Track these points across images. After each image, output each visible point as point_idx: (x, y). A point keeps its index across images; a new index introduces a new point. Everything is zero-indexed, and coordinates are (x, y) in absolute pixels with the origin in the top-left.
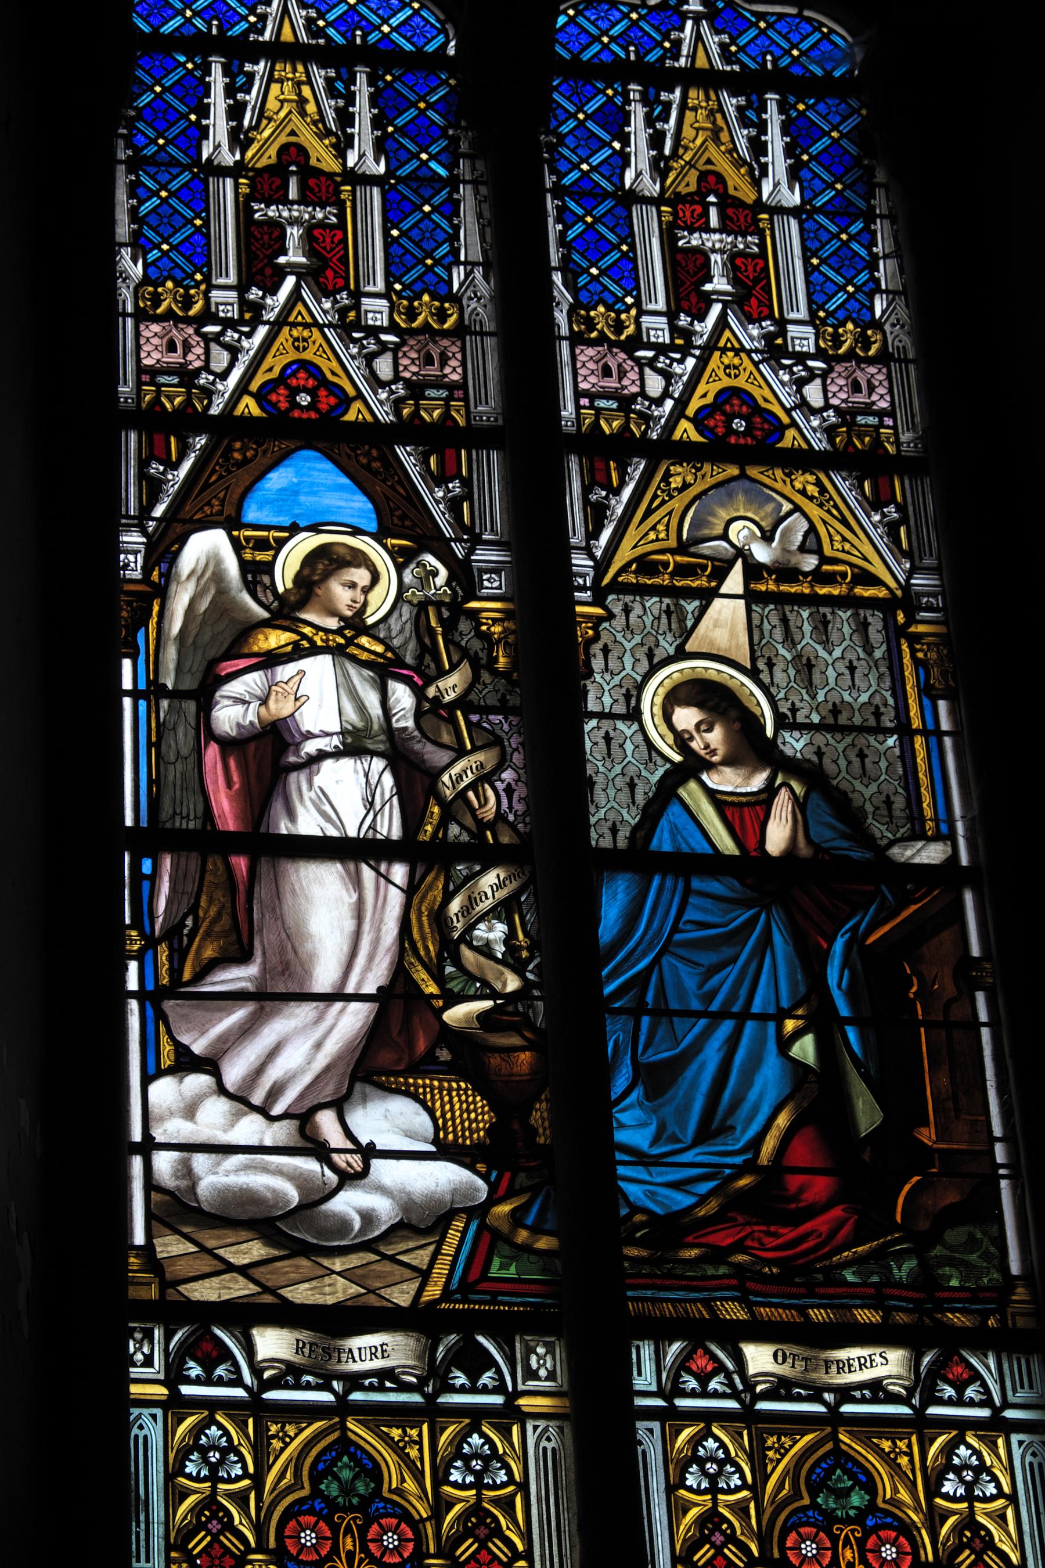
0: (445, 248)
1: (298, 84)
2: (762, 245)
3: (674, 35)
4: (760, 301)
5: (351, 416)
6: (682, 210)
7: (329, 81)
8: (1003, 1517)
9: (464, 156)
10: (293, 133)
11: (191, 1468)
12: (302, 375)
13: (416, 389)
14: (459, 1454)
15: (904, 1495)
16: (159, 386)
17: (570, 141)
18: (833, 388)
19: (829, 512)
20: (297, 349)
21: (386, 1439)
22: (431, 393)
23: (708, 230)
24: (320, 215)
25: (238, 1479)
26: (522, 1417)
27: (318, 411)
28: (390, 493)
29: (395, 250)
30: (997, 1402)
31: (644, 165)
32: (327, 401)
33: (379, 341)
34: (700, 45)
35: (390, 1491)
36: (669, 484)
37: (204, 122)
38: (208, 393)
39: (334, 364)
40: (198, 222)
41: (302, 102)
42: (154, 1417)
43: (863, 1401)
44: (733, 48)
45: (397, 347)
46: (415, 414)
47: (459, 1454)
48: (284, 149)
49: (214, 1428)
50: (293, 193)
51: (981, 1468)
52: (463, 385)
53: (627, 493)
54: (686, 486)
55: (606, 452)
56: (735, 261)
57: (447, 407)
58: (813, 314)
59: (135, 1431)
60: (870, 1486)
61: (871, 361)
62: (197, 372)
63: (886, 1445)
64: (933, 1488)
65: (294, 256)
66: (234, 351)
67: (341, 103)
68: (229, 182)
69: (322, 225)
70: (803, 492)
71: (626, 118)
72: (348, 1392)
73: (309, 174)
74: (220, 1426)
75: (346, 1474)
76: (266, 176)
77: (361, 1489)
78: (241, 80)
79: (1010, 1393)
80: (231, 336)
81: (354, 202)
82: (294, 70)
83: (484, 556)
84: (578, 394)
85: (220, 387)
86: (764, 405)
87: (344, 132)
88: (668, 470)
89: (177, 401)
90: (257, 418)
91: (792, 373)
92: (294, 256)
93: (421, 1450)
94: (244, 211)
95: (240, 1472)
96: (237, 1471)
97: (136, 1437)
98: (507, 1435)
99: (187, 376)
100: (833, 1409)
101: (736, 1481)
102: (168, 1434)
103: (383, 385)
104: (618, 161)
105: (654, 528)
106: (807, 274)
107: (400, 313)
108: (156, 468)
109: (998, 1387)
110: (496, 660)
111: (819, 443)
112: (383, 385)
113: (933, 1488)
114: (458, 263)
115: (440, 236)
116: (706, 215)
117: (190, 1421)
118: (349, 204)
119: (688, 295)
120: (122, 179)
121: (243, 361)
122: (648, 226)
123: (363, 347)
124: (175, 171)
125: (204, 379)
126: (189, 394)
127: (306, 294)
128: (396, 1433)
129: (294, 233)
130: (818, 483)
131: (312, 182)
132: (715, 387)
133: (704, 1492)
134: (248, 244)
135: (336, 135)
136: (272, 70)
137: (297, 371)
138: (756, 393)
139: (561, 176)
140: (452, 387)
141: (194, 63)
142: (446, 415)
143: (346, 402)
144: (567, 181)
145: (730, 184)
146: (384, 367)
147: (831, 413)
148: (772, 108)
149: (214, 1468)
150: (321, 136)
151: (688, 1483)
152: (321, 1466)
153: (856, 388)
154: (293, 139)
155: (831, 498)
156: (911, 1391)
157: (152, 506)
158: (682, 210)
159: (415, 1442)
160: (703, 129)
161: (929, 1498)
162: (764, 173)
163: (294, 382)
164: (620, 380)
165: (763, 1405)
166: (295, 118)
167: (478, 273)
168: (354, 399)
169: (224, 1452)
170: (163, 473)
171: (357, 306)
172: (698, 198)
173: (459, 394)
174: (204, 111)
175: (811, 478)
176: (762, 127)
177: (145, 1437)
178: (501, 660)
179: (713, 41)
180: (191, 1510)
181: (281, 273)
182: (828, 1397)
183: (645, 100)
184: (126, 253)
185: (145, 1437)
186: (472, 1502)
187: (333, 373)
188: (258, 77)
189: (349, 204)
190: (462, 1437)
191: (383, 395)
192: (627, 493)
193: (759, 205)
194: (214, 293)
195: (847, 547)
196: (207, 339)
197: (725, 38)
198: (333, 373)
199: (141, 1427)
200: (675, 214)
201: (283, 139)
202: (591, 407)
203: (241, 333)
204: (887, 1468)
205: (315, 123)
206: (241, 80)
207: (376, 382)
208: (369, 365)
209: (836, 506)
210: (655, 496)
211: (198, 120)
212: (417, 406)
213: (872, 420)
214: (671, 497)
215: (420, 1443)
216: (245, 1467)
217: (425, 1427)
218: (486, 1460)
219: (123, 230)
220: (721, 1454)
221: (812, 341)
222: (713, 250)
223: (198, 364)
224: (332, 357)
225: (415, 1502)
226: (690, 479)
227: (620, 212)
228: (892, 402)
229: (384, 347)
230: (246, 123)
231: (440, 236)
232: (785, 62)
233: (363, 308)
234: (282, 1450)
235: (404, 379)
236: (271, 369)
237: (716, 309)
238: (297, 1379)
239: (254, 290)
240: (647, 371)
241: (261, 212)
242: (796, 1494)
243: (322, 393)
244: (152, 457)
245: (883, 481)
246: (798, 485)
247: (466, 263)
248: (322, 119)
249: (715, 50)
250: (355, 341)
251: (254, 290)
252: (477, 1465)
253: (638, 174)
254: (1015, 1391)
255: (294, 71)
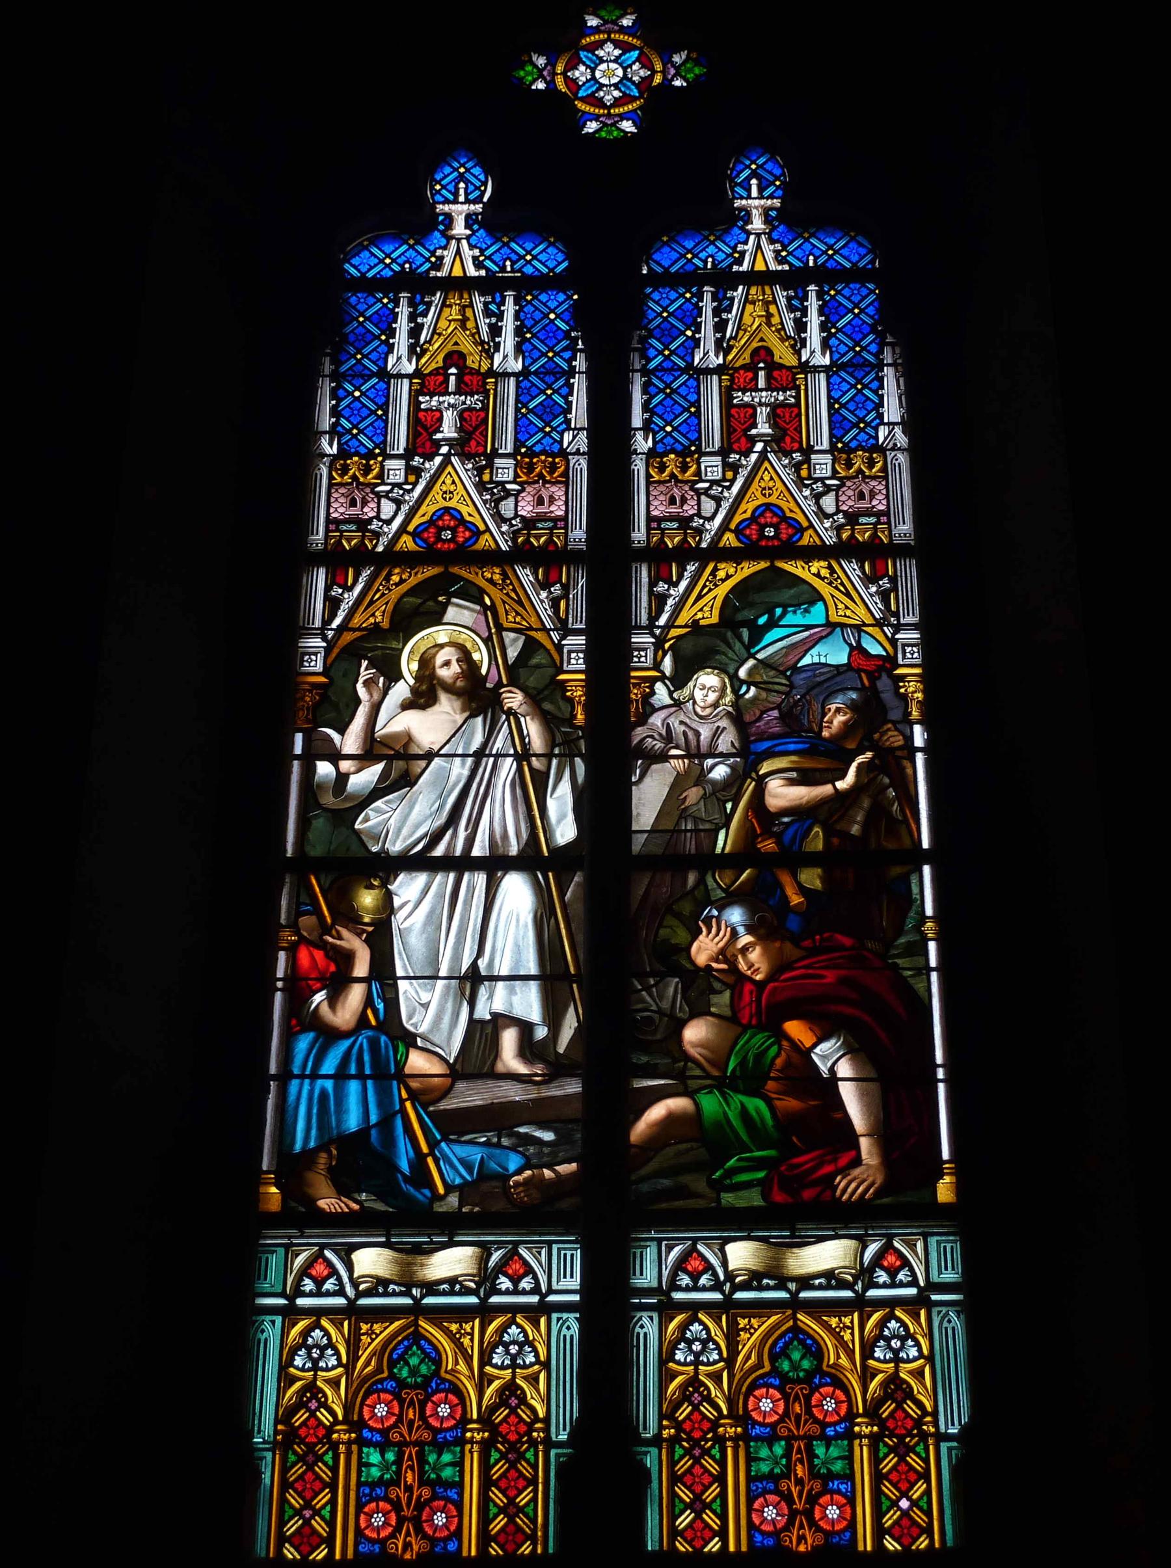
0: (873, 415)
1: (767, 304)
2: (797, 397)
3: (740, 248)
4: (792, 438)
5: (805, 541)
6: (735, 377)
7: (789, 299)
8: (537, 1380)
9: (581, 351)
10: (456, 344)
11: (679, 1356)
12: (768, 515)
13: (852, 518)
14: (682, 1338)
15: (844, 1361)
16: (342, 532)
17: (866, 329)
18: (843, 498)
19: (836, 588)
20: (764, 495)
21: (827, 1327)
22: (863, 520)
23: (757, 390)
24: (781, 398)
25: (715, 1362)
26: (930, 1305)
27: (780, 540)
28: (505, 598)
29: (836, 418)
30: (922, 1284)
31: (711, 345)
32: (785, 533)
33: (825, 485)
34: (458, 258)
35: (446, 1372)
36: (715, 576)
37: (391, 341)
38: (699, 531)
39: (792, 505)
40: (380, 412)
41: (769, 316)
42: (651, 1318)
43: (820, 1287)
44: (482, 258)
45: (839, 487)
46: (852, 536)
47: (304, 1344)
48: (755, 352)
49: (893, 1322)
50: (761, 383)
51: (909, 1335)
52: (886, 513)
53: (683, 585)
54: (402, 581)
55: (663, 560)
56: (776, 410)
57: (875, 530)
58: (833, 445)
59: (637, 1329)
60: (438, 1361)
61: (874, 478)
62: (691, 518)
63: (834, 1322)
64: (867, 1352)
65: (763, 428)
66: (718, 500)
67: (494, 320)
68: (715, 377)
69: (783, 405)
70: (818, 575)
71: (395, 317)
72: (798, 1291)
73: (773, 367)
74: (701, 1323)
75: (414, 1361)
76: (742, 372)
77: (424, 1369)
78: (421, 308)
79: (554, 1279)
80: (397, 492)
81: (495, 390)
82: (461, 298)
83: (570, 641)
84: (329, 520)
85: (708, 527)
86: (788, 514)
87: (800, 337)
88: (716, 566)
89: (676, 540)
90: (412, 552)
91: (493, 494)
92: (763, 428)
93: (852, 1334)
94: (414, 404)
95: (717, 1357)
96: (333, 1361)
97: (638, 1334)
98: (536, 1325)
99: (684, 522)
100: (795, 1295)
101: (913, 1352)
102: (284, 1334)
103: (827, 516)
104: (691, 343)
105: (701, 610)
106: (516, 420)
107: (840, 464)
108: (337, 591)
109: (923, 1269)
110: (575, 717)
111: (830, 539)
112: (827, 516)
113: (867, 1352)
114: (569, 428)
115: (557, 410)
116: (447, 381)
117: (876, 1316)
118: (803, 387)
119: (739, 439)
120: (326, 386)
121: (726, 505)
122: (713, 388)
123: (813, 489)
124: (676, 374)
125: (374, 526)
126: (685, 534)
127: (771, 456)
128: (834, 1322)
129: (762, 414)
130: (830, 567)
131: (776, 374)
132: (433, 508)
133: (309, 1370)
134: (728, 421)
135: (794, 338)
136: (748, 294)
137: (442, 515)
138: (465, 510)
139: (649, 360)
140: (879, 514)
141: (389, 298)
142: (874, 535)
143: (477, 534)
144: (344, 368)
145: (775, 352)
146: (828, 503)
147: (840, 515)
148: (812, 296)
149: (697, 1355)
150: (782, 340)
151: (677, 1357)
152: (395, 1356)
153: (861, 496)
154: (456, 348)
155: (839, 577)
156: (856, 1278)
157: (657, 618)
158: (735, 377)
159: (848, 1328)
160: (454, 320)
161: (482, 1365)
162: (804, 345)
163: (762, 521)
164: (682, 506)
165: (739, 1295)
166: (765, 328)
167: (898, 430)
168: (807, 528)
169: (903, 1339)
170: (341, 595)
171: (808, 461)
172: (752, 368)
173: (561, 524)
174: (392, 333)
175: (824, 564)
176: (500, 316)
177: (645, 1334)
178: (579, 716)
179: (768, 250)
180: (297, 1392)
181: (753, 440)
182: (792, 1286)
183: (412, 303)
184: (639, 436)
185: (645, 1334)
186: (508, 1378)
187: (470, 515)
188: (736, 301)
189: (803, 387)
190: (503, 1329)
191: (827, 524)
192: (683, 585)
193: (491, 372)
194: (387, 462)
195: (848, 613)
196: (699, 493)
197: (778, 247)
198: (791, 511)
199: (642, 1327)
200: (732, 380)
201: (755, 345)
202: (659, 528)
203: (724, 487)
204: (452, 1345)
205: (778, 331)
206: (421, 308)
207: (822, 514)
208: (817, 503)
209: (842, 584)
210: (705, 586)
211: (693, 335)
212: (853, 530)
213: (873, 520)
214: (716, 586)
215: (852, 1328)
216: (720, 1353)
217: (856, 1315)
218: (704, 1343)
219: (637, 421)
220: (902, 1332)
221: (829, 467)
222: (761, 404)
223: (691, 512)
224: (790, 499)
225: (849, 1376)
226: (732, 571)
227: (382, 385)
228: (567, 512)
229: (828, 489)
230: (728, 335)
231: (870, 406)
232: (820, 261)
233: (496, 465)
234: (370, 1344)
235: (843, 511)
236: (745, 512)
237: (759, 446)
238: (760, 1282)
239: (417, 458)
240: (703, 497)
241: (740, 397)
242: (378, 1370)
243: (783, 526)
244: (334, 583)
245: (879, 564)
246: (814, 570)
247: (575, 429)
248: (783, 328)
249: (770, 256)
250: (807, 486)
251: (417, 458)
252: (697, 1347)
253: (707, 355)
254: (940, 1273)
255: (764, 294)
